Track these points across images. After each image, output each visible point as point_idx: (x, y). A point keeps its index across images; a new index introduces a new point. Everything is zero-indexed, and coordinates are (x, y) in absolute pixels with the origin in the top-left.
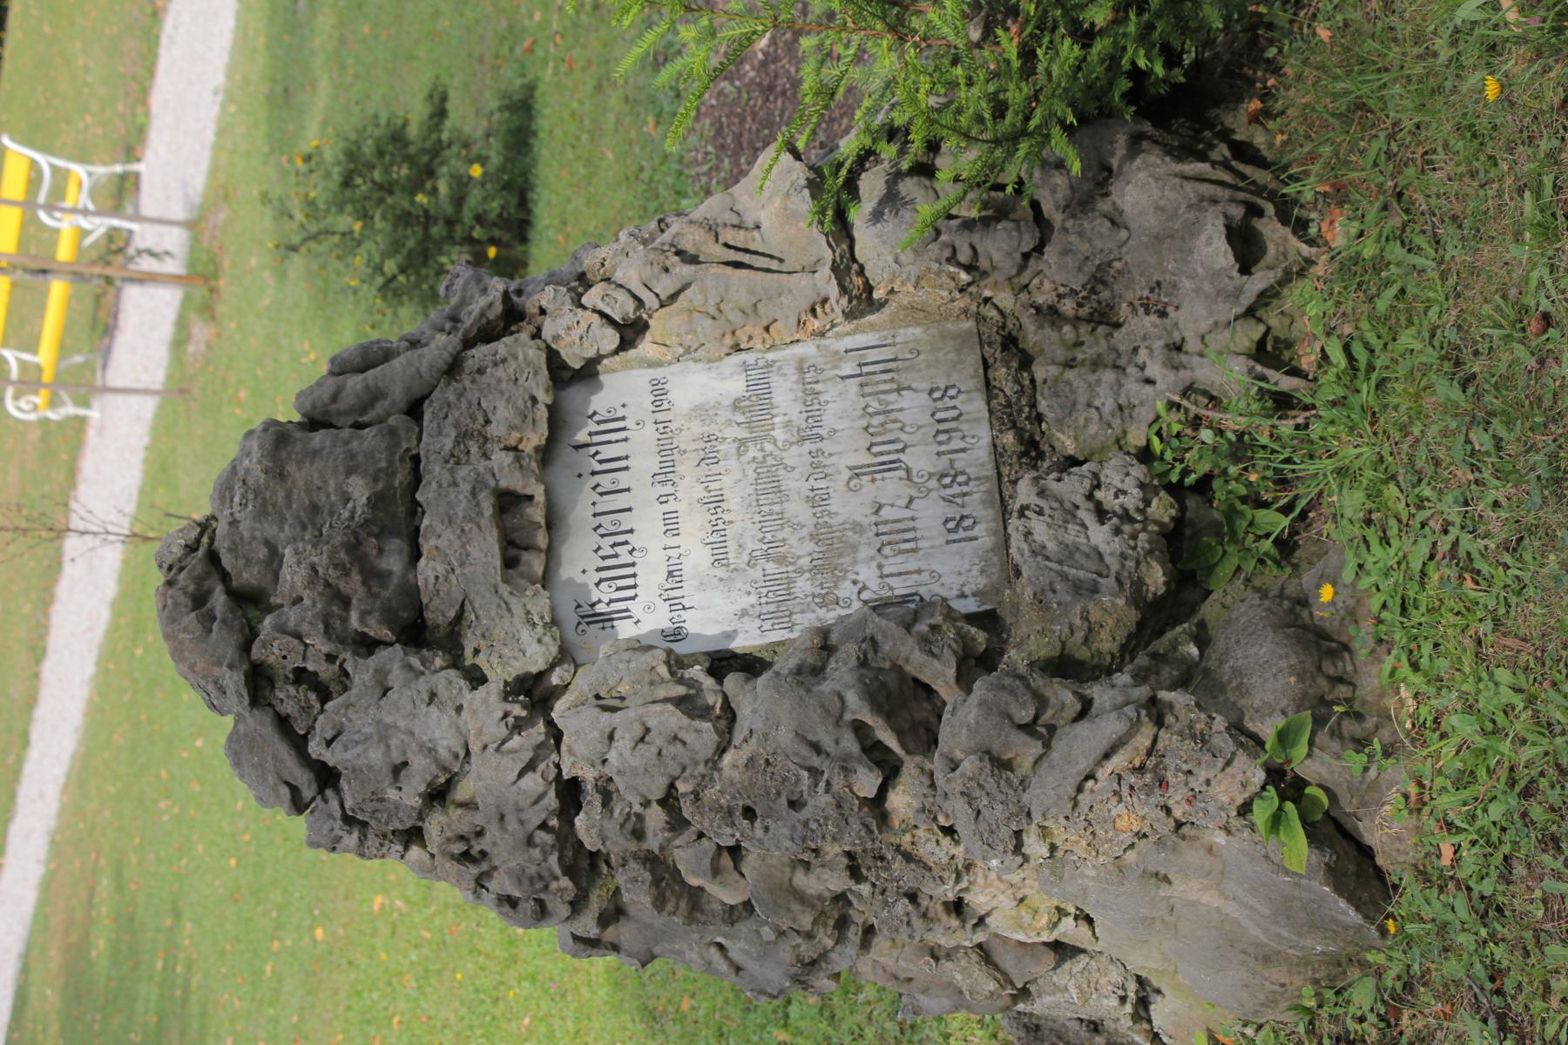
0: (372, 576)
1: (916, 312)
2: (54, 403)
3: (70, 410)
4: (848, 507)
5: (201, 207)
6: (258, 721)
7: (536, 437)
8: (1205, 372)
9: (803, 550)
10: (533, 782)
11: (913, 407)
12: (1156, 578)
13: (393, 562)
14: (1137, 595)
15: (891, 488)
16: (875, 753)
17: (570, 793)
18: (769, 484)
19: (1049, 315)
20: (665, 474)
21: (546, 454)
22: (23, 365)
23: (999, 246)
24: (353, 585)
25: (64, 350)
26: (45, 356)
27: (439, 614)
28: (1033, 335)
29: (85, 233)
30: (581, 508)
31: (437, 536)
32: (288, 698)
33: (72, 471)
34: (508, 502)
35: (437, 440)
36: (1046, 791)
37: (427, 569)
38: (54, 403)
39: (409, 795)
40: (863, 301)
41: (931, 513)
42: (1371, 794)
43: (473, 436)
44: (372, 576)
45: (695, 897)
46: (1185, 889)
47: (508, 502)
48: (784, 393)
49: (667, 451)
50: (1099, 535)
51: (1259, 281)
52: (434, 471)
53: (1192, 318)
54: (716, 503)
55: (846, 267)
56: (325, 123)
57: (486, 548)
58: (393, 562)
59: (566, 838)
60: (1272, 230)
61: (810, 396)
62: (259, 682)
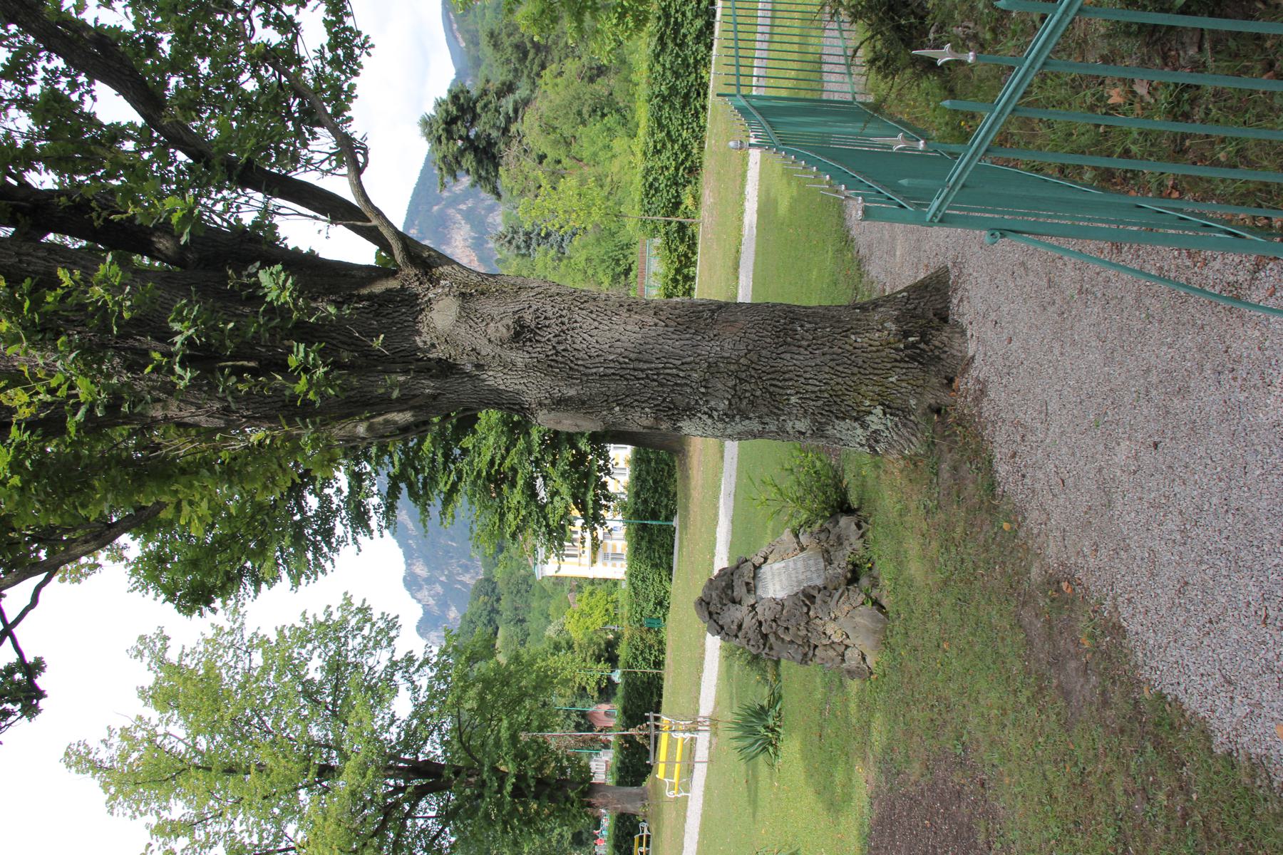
0: (726, 594)
1: (811, 549)
2: (679, 792)
3: (683, 794)
4: (801, 577)
5: (687, 471)
6: (712, 622)
7: (752, 575)
8: (855, 547)
9: (795, 584)
10: (754, 621)
11: (811, 562)
12: (849, 575)
13: (730, 592)
14: (846, 577)
15: (809, 573)
16: (806, 605)
17: (760, 623)
18: (789, 575)
19: (833, 546)
20: (773, 578)
21: (754, 578)
22: (670, 783)
23: (823, 536)
24: (723, 596)
25: (680, 778)
26: (675, 780)
27: (737, 600)
28: (830, 549)
29: (684, 739)
30: (760, 585)
31: (736, 589)
32: (715, 616)
33: (685, 817)
34: (747, 584)
35: (736, 577)
36: (833, 604)
37: (735, 594)
38: (679, 792)
39: (734, 627)
40: (803, 549)
41: (815, 576)
42: (881, 596)
43: (742, 575)
44: (726, 594)
45: (783, 639)
46: (858, 619)
47: (747, 584)
48: (791, 564)
49: (773, 575)
50: (839, 571)
51: (861, 532)
52: (736, 581)
53: (853, 539)
54: (781, 581)
55: (799, 543)
56: (637, 126)
57: (744, 589)
58: (730, 592)
59: (760, 631)
60: (863, 524)
61: (795, 564)
62: (710, 614)
